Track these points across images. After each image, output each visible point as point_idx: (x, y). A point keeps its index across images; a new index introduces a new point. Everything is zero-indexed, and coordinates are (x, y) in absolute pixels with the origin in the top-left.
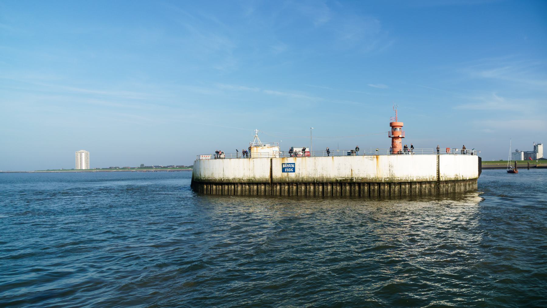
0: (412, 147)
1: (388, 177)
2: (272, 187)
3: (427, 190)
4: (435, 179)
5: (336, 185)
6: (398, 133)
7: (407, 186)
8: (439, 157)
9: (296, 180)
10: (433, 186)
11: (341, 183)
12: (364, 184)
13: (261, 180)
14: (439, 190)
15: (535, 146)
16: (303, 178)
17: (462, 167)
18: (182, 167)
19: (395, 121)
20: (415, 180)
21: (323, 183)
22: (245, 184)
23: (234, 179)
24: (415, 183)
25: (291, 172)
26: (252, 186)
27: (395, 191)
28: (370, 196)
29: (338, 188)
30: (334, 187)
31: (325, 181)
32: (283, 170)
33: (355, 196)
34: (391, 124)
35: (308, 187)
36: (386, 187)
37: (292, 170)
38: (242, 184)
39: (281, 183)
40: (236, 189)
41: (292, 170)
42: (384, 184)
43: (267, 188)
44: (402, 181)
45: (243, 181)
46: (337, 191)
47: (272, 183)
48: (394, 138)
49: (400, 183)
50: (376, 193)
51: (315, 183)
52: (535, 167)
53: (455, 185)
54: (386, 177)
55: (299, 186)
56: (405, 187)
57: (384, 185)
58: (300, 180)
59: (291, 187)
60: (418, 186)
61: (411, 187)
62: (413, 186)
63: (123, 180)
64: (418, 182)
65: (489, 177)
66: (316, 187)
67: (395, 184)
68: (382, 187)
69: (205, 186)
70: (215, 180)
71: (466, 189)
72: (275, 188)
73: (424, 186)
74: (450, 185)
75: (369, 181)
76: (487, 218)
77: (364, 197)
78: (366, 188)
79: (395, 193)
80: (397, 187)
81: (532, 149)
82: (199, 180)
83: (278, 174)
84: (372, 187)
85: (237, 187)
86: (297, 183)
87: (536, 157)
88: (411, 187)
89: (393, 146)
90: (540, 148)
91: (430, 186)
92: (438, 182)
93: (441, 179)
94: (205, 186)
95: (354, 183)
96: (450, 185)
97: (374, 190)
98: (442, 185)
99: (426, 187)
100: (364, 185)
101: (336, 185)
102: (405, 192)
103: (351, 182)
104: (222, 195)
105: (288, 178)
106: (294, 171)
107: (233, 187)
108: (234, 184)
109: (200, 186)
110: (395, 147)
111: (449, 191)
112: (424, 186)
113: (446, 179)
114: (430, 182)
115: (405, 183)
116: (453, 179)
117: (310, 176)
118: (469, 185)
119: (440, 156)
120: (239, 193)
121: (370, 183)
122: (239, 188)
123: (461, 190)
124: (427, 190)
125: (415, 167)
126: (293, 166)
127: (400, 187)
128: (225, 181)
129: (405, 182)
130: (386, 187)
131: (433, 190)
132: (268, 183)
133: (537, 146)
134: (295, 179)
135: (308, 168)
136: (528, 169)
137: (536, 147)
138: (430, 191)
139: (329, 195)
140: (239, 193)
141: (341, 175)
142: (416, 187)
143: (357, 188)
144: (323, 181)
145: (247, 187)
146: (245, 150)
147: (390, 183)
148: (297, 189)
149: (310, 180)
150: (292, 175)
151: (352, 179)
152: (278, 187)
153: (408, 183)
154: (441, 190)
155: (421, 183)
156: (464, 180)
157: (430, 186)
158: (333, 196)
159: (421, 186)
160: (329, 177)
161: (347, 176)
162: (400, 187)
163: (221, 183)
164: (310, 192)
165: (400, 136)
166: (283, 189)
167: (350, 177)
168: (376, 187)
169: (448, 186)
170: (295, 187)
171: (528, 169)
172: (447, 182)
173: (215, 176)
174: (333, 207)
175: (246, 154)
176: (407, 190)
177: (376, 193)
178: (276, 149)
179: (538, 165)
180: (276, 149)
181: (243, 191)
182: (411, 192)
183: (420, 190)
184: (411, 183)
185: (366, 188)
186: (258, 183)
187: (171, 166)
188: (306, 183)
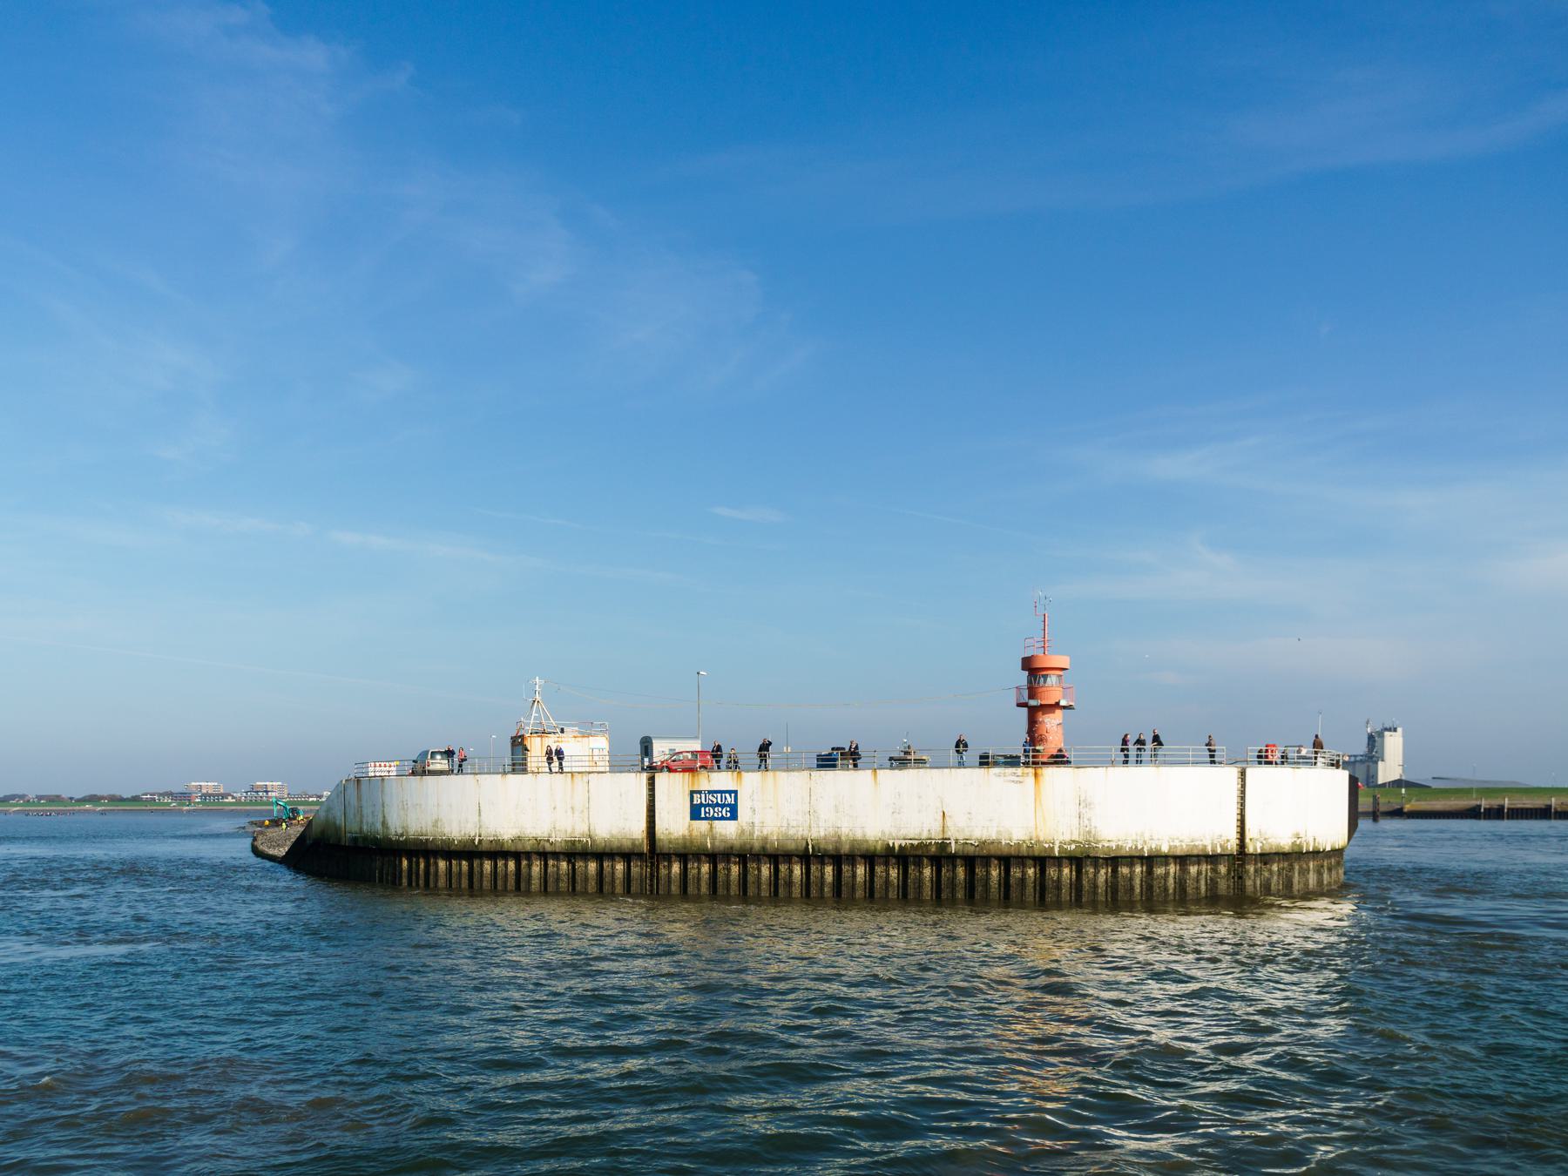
0: (1156, 739)
1: (1075, 837)
2: (655, 868)
3: (1203, 882)
4: (1232, 845)
5: (887, 864)
6: (1053, 689)
7: (1138, 869)
8: (1243, 774)
9: (742, 847)
10: (1223, 869)
11: (905, 857)
12: (986, 860)
13: (616, 844)
14: (1237, 880)
15: (1371, 738)
16: (765, 839)
17: (1304, 808)
18: (54, 799)
19: (1040, 653)
20: (1165, 849)
21: (840, 857)
22: (556, 855)
23: (519, 839)
24: (1165, 859)
25: (722, 818)
26: (579, 864)
27: (1095, 886)
28: (938, 896)
29: (894, 873)
30: (879, 869)
31: (845, 849)
32: (695, 813)
33: (822, 897)
34: (1028, 665)
35: (783, 868)
36: (1066, 871)
37: (725, 812)
38: (544, 855)
39: (687, 854)
40: (524, 870)
41: (725, 812)
42: (1058, 861)
43: (635, 870)
44: (1123, 853)
45: (548, 848)
46: (887, 881)
47: (652, 852)
48: (1034, 713)
49: (1114, 861)
50: (1030, 890)
51: (809, 856)
52: (1398, 813)
53: (1291, 869)
54: (1067, 838)
55: (752, 866)
56: (1132, 872)
57: (1060, 866)
58: (757, 845)
59: (720, 866)
60: (1172, 869)
61: (1150, 872)
62: (1159, 871)
63: (29, 839)
64: (1176, 858)
65: (1395, 844)
66: (813, 868)
67: (1096, 861)
68: (1052, 872)
69: (405, 863)
70: (450, 842)
71: (1320, 882)
72: (663, 872)
73: (1193, 870)
74: (1275, 868)
75: (1006, 851)
76: (1365, 978)
77: (986, 900)
78: (995, 873)
79: (1095, 893)
80: (1103, 871)
81: (1361, 748)
82: (376, 841)
83: (675, 824)
84: (1016, 872)
85: (529, 866)
86: (745, 855)
87: (1375, 776)
88: (1150, 872)
89: (1034, 736)
90: (1393, 744)
91: (1214, 870)
92: (1241, 856)
93: (1250, 849)
94: (405, 863)
95: (953, 858)
96: (1275, 868)
97: (1023, 880)
98: (1251, 868)
99: (1199, 873)
100: (919, 865)
101: (887, 864)
102: (1132, 888)
103: (940, 856)
104: (473, 889)
105: (713, 838)
106: (734, 816)
107: (511, 865)
108: (517, 856)
109: (347, 858)
110: (1042, 740)
111: (1273, 887)
112: (1193, 870)
113: (1267, 849)
114: (1212, 859)
115: (1131, 860)
116: (1287, 849)
117: (791, 832)
118: (1330, 870)
119: (1249, 771)
120: (536, 884)
121: (1008, 860)
122: (536, 868)
123: (1306, 884)
124: (1203, 882)
125: (1167, 808)
126: (730, 800)
127: (1115, 871)
128: (485, 847)
129: (1132, 857)
130: (1066, 871)
131: (1222, 886)
132: (640, 855)
133: (1381, 734)
134: (737, 843)
135: (784, 806)
136: (1375, 820)
137: (1374, 741)
138: (1212, 884)
139: (859, 893)
140: (536, 884)
141: (903, 832)
142: (1167, 874)
143: (961, 872)
144: (837, 849)
145: (564, 865)
146: (726, 750)
147: (1079, 860)
148: (685, 871)
149: (791, 846)
150: (727, 831)
151: (943, 845)
152: (676, 868)
153: (1141, 858)
154: (1249, 883)
155: (1183, 860)
156: (1316, 854)
157: (1214, 870)
158: (873, 898)
159: (1184, 870)
160: (859, 835)
161: (925, 835)
162: (1115, 871)
163: (471, 852)
164: (790, 884)
165: (1063, 703)
166: (692, 872)
167: (937, 835)
168: (1031, 871)
169: (1270, 871)
170: (735, 870)
171: (1375, 820)
172: (1266, 858)
173: (446, 831)
174: (897, 937)
175: (517, 758)
176: (1137, 882)
177: (1030, 890)
178: (601, 743)
179: (1407, 808)
180: (601, 743)
181: (551, 880)
182: (1150, 888)
183: (1181, 884)
184: (1151, 860)
185: (995, 873)
186: (603, 854)
187: (22, 797)
188: (777, 856)
